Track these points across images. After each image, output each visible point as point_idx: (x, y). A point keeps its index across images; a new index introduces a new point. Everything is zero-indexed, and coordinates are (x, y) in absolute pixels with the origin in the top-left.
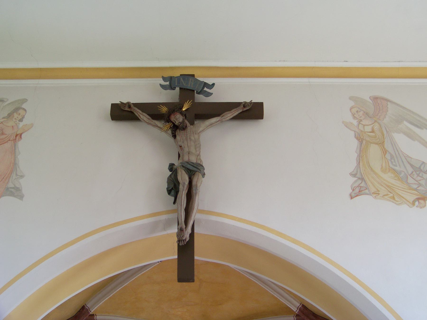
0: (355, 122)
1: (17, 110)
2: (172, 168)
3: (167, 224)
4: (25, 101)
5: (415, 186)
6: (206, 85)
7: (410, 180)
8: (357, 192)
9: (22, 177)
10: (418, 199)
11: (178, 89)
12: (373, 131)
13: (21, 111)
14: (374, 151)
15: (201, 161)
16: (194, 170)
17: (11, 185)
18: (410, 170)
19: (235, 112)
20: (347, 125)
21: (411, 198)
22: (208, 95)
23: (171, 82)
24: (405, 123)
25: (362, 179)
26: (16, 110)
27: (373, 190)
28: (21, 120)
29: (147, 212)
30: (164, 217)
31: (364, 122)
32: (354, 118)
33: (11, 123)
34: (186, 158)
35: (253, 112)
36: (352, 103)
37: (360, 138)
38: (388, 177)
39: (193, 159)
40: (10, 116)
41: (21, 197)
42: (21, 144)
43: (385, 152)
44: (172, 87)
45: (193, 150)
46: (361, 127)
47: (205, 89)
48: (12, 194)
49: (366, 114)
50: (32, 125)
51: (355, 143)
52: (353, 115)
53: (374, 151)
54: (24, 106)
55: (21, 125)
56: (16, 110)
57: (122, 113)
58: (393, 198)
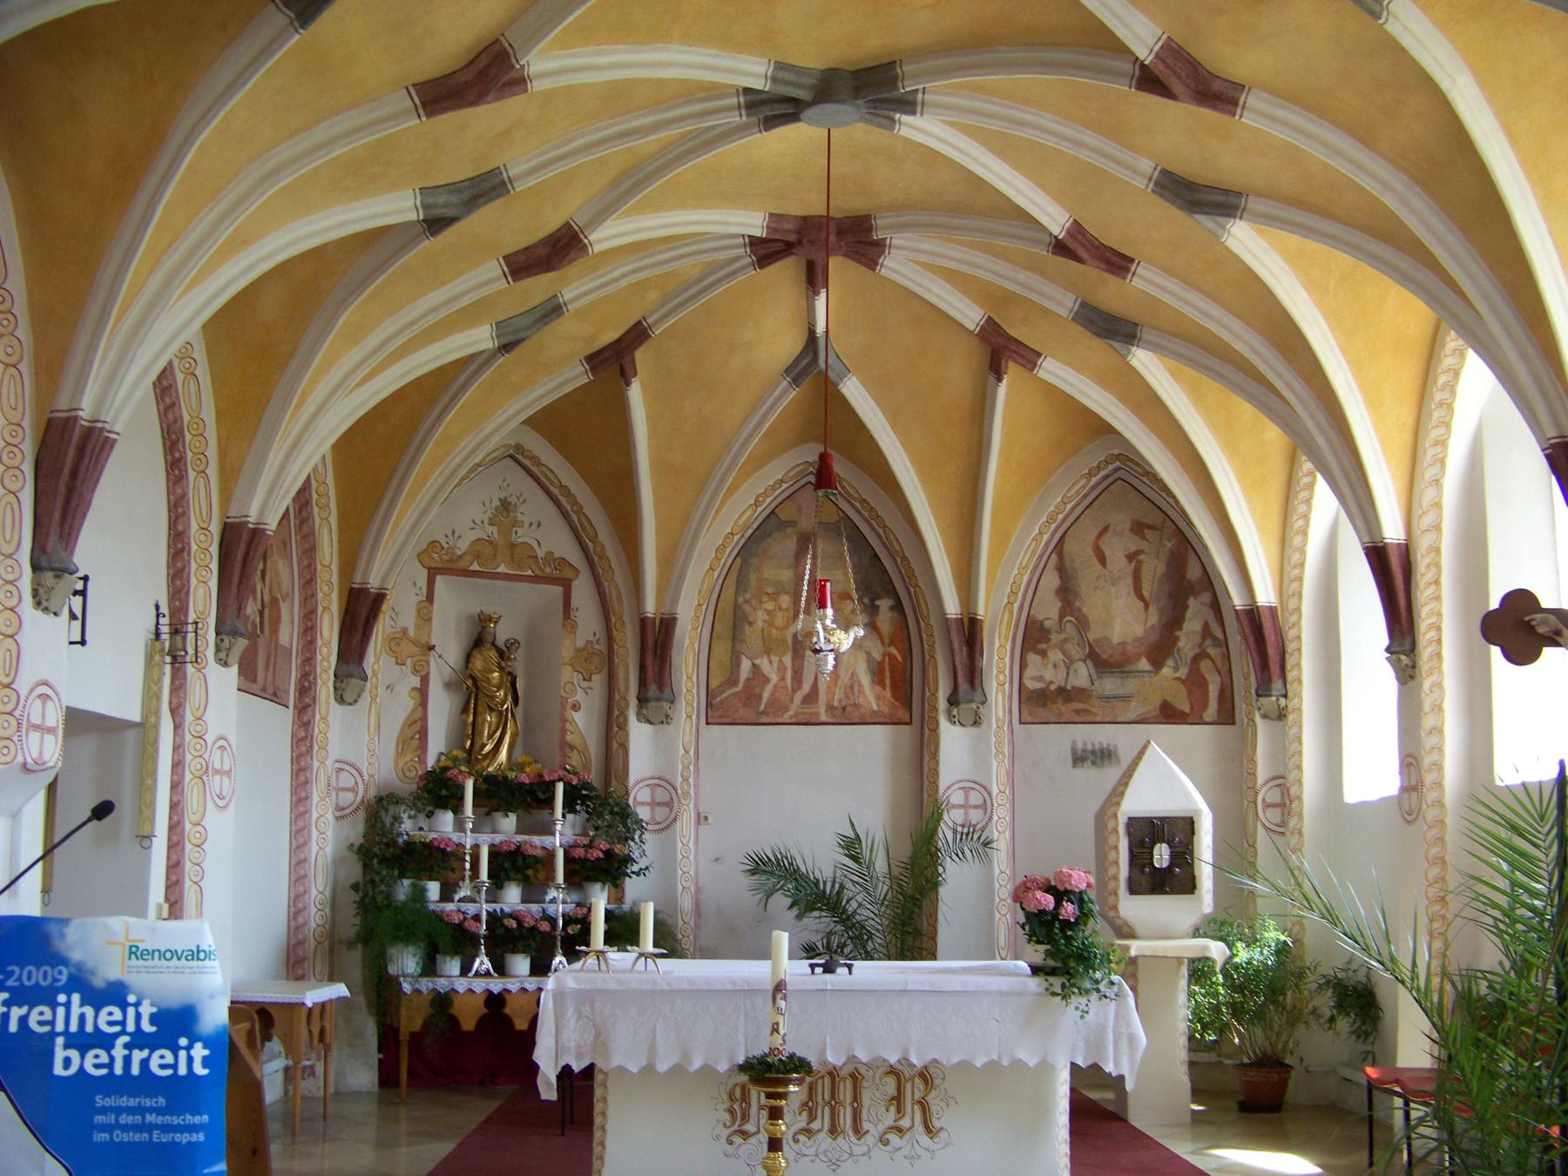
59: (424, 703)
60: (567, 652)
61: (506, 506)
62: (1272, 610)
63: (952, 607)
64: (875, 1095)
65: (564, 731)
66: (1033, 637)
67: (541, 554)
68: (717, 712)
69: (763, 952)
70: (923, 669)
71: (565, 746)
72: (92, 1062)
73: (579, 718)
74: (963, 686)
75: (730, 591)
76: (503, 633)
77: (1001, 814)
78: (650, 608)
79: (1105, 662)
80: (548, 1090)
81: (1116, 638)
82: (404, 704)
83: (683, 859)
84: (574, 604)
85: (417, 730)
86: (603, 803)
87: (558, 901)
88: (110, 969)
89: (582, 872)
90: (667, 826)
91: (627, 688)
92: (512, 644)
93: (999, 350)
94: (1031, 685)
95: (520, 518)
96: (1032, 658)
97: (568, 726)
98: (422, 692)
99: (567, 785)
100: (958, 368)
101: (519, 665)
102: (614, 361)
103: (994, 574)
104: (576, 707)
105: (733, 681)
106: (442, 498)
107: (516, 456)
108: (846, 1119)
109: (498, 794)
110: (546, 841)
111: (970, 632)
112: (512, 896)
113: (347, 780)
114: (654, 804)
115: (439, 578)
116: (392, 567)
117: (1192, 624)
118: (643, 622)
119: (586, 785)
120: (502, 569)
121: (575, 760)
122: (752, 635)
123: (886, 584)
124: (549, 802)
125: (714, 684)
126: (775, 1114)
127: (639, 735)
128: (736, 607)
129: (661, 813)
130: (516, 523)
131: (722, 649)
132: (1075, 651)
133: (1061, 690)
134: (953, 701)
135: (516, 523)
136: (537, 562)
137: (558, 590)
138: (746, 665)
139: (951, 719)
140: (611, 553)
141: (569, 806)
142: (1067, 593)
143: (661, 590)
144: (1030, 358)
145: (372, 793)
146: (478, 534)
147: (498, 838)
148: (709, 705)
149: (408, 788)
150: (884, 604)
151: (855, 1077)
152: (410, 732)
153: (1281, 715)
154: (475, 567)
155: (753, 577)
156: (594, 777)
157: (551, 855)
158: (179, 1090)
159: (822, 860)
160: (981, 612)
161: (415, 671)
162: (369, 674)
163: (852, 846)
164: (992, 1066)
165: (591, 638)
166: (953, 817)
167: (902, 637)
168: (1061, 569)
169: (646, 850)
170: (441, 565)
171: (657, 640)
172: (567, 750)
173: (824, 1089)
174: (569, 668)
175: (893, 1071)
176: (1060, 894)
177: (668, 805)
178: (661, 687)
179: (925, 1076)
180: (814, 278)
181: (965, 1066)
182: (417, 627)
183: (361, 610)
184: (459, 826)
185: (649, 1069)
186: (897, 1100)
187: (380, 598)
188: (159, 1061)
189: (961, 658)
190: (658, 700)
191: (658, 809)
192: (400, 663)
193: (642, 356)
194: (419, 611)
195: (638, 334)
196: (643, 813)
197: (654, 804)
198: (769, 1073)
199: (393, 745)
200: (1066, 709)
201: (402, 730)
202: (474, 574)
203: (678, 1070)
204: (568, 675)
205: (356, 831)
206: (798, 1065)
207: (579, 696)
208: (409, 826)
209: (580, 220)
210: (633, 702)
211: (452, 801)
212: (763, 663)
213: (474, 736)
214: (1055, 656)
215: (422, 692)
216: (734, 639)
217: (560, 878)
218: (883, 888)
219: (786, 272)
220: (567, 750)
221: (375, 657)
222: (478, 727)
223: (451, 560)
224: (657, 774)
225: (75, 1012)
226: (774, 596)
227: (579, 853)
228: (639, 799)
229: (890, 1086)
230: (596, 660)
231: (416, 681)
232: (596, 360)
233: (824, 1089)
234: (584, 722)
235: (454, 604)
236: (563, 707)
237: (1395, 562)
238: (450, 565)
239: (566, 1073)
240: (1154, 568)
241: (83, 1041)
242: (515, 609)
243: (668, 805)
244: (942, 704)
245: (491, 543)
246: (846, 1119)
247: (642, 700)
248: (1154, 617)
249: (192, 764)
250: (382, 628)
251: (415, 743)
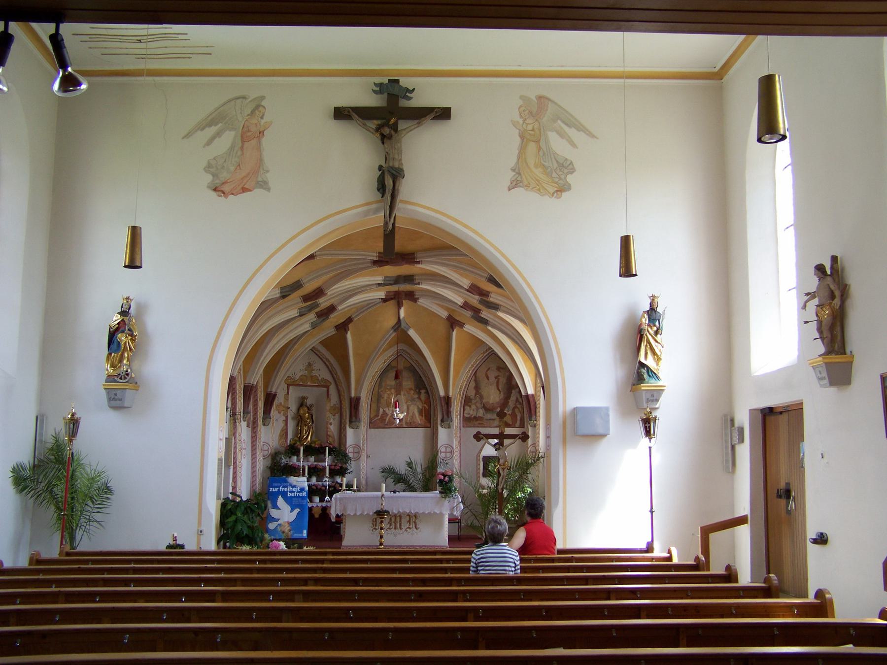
0: (521, 121)
1: (258, 107)
2: (380, 168)
3: (376, 211)
4: (263, 98)
5: (557, 180)
6: (407, 90)
7: (554, 175)
8: (515, 184)
9: (268, 171)
10: (557, 191)
11: (386, 95)
12: (533, 130)
13: (261, 109)
14: (532, 147)
15: (402, 164)
16: (397, 174)
17: (260, 179)
18: (555, 165)
19: (433, 115)
20: (515, 124)
21: (552, 190)
22: (410, 98)
23: (380, 89)
24: (559, 121)
25: (519, 174)
26: (258, 107)
27: (526, 183)
28: (262, 118)
29: (362, 202)
30: (374, 206)
31: (529, 121)
32: (521, 116)
33: (254, 121)
34: (391, 164)
35: (444, 114)
36: (521, 102)
37: (522, 137)
38: (538, 172)
39: (396, 165)
40: (253, 112)
41: (268, 189)
42: (264, 141)
43: (539, 149)
44: (380, 92)
45: (396, 157)
46: (525, 125)
47: (408, 94)
48: (261, 187)
49: (531, 113)
50: (271, 123)
51: (518, 140)
52: (520, 114)
53: (532, 147)
54: (263, 103)
55: (263, 121)
56: (258, 107)
57: (340, 114)
58: (539, 190)
59: (286, 424)
60: (328, 408)
61: (310, 365)
62: (533, 395)
63: (442, 393)
64: (404, 520)
66: (467, 401)
68: (373, 425)
69: (379, 490)
70: (433, 411)
71: (328, 435)
72: (292, 495)
73: (331, 427)
74: (445, 416)
75: (376, 389)
76: (309, 402)
77: (456, 455)
78: (353, 395)
79: (487, 409)
80: (333, 520)
81: (491, 402)
82: (281, 425)
83: (363, 467)
85: (285, 432)
86: (339, 453)
87: (327, 481)
88: (294, 483)
89: (334, 473)
90: (358, 459)
92: (311, 406)
93: (453, 323)
94: (466, 415)
96: (467, 407)
98: (286, 421)
100: (442, 328)
101: (314, 412)
102: (343, 327)
103: (454, 382)
104: (331, 424)
105: (377, 415)
106: (294, 366)
107: (313, 350)
108: (398, 525)
109: (310, 451)
110: (323, 464)
111: (447, 400)
112: (314, 480)
113: (266, 448)
114: (354, 453)
116: (278, 387)
117: (513, 398)
118: (351, 399)
119: (334, 447)
121: (331, 440)
122: (383, 401)
123: (422, 384)
124: (324, 453)
126: (382, 522)
127: (350, 432)
129: (356, 455)
131: (374, 405)
132: (479, 405)
133: (475, 417)
134: (442, 421)
137: (325, 389)
138: (381, 410)
139: (442, 426)
141: (330, 454)
142: (477, 388)
143: (356, 389)
144: (461, 325)
145: (273, 451)
146: (302, 373)
147: (310, 464)
149: (283, 450)
150: (423, 391)
151: (400, 517)
153: (535, 426)
155: (383, 384)
156: (336, 445)
157: (325, 468)
158: (303, 498)
159: (402, 469)
160: (451, 394)
163: (410, 464)
164: (429, 513)
166: (441, 455)
167: (428, 401)
168: (476, 381)
169: (352, 466)
170: (291, 383)
171: (355, 404)
173: (393, 519)
175: (408, 515)
176: (445, 476)
177: (358, 452)
179: (416, 516)
180: (399, 305)
181: (423, 513)
183: (270, 399)
184: (298, 460)
185: (355, 515)
186: (409, 521)
187: (275, 395)
188: (300, 494)
189: (445, 408)
192: (280, 413)
193: (350, 326)
195: (350, 320)
196: (351, 455)
197: (354, 453)
198: (380, 513)
200: (477, 423)
203: (361, 514)
204: (329, 415)
205: (269, 462)
206: (388, 512)
207: (332, 421)
208: (284, 460)
209: (336, 303)
211: (297, 453)
212: (386, 410)
213: (301, 433)
214: (473, 407)
215: (286, 421)
217: (327, 474)
218: (420, 476)
219: (392, 304)
221: (274, 412)
225: (290, 488)
226: (390, 389)
227: (333, 467)
229: (408, 518)
232: (338, 327)
233: (393, 519)
234: (333, 428)
235: (295, 394)
237: (531, 399)
239: (337, 516)
240: (503, 380)
241: (291, 492)
242: (312, 395)
244: (439, 422)
246: (398, 525)
247: (351, 422)
248: (502, 396)
249: (238, 447)
250: (276, 402)
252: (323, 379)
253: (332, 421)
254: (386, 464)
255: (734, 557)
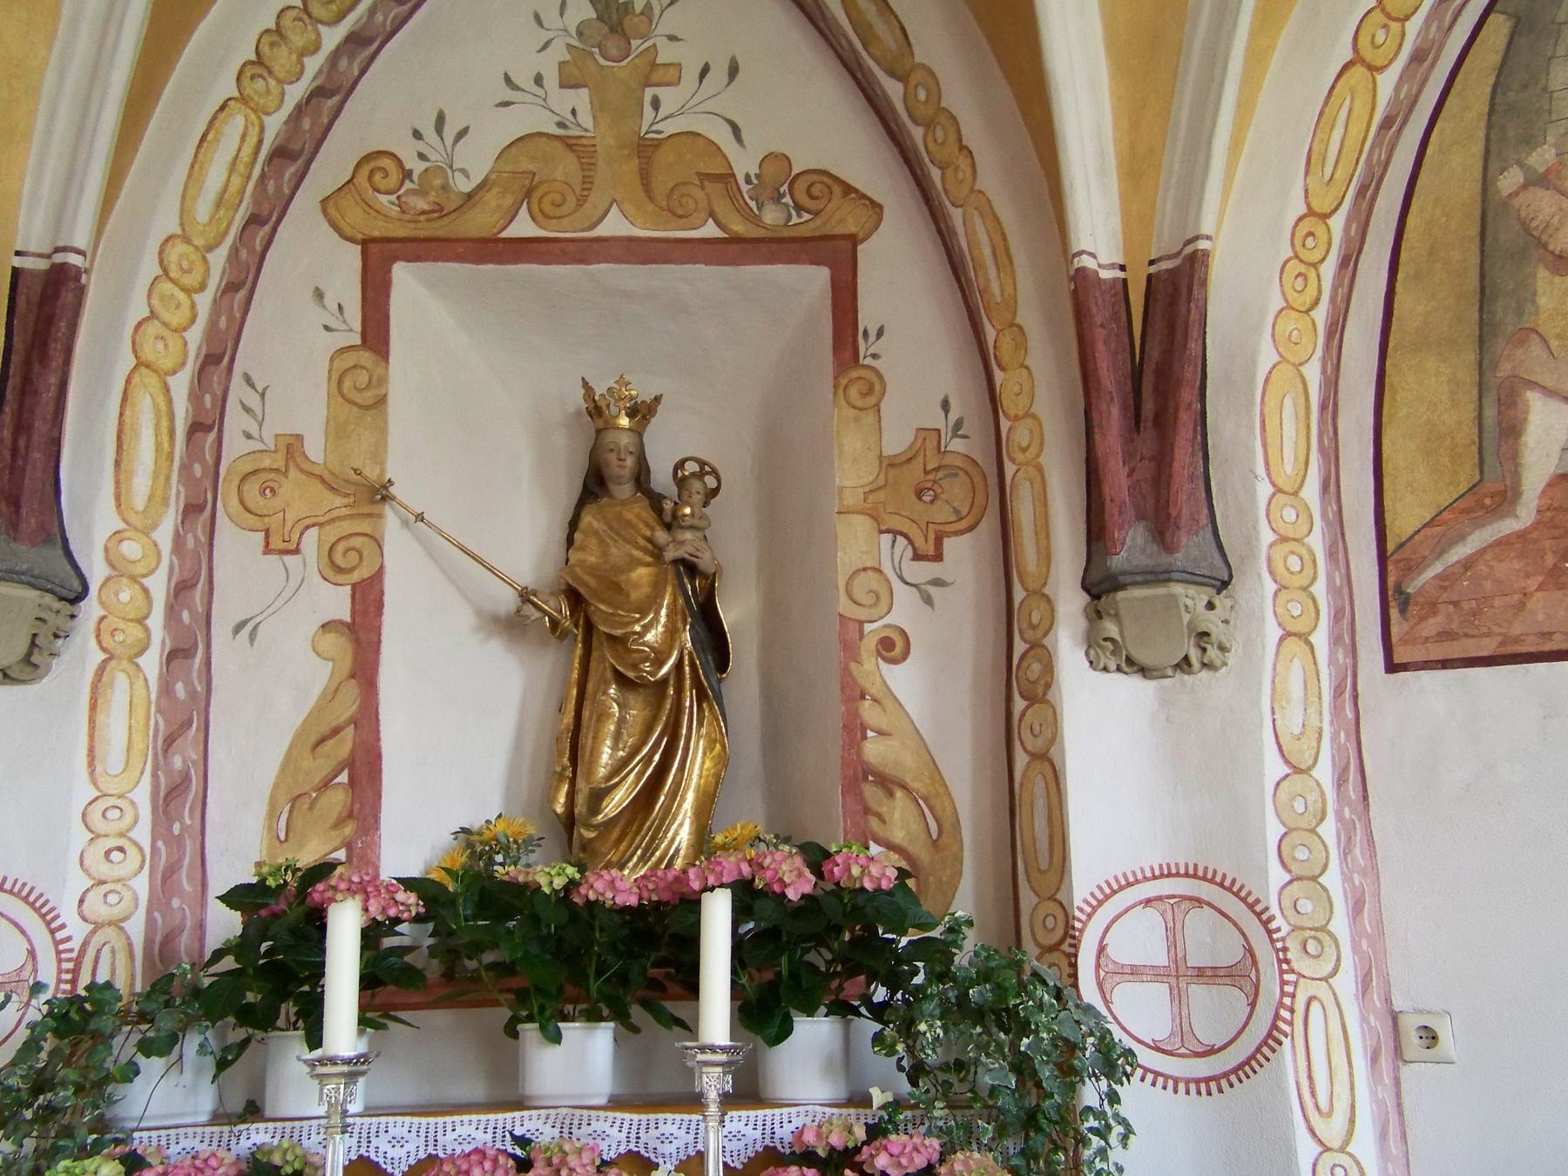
59: (364, 669)
60: (852, 473)
65: (855, 731)
67: (744, 164)
68: (1425, 614)
73: (905, 682)
75: (1458, 160)
84: (868, 316)
90: (1234, 1072)
91: (1046, 558)
95: (667, 53)
97: (867, 710)
99: (747, 898)
104: (893, 648)
105: (1490, 494)
114: (1180, 974)
115: (402, 273)
120: (615, 225)
125: (1403, 522)
127: (1103, 722)
128: (1490, 212)
129: (1214, 1011)
130: (653, 73)
131: (1435, 389)
135: (653, 73)
136: (733, 193)
137: (815, 279)
140: (959, 96)
143: (1138, 169)
148: (1391, 597)
152: (320, 767)
154: (523, 227)
161: (334, 569)
162: (96, 571)
165: (936, 419)
171: (1144, 359)
172: (871, 792)
174: (861, 524)
178: (1163, 528)
182: (337, 431)
190: (1158, 576)
191: (1198, 993)
194: (338, 381)
196: (1138, 1014)
199: (259, 810)
201: (289, 764)
202: (523, 250)
204: (856, 544)
207: (904, 611)
210: (1070, 602)
216: (1486, 334)
220: (871, 792)
222: (586, 740)
223: (439, 211)
224: (1181, 859)
228: (1123, 950)
230: (956, 491)
231: (338, 603)
234: (923, 698)
236: (850, 650)
238: (439, 229)
243: (1239, 974)
245: (570, 144)
247: (1100, 587)
251: (337, 799)
252: (779, 177)
253: (904, 611)
254: (322, 288)
255: (757, 1082)
